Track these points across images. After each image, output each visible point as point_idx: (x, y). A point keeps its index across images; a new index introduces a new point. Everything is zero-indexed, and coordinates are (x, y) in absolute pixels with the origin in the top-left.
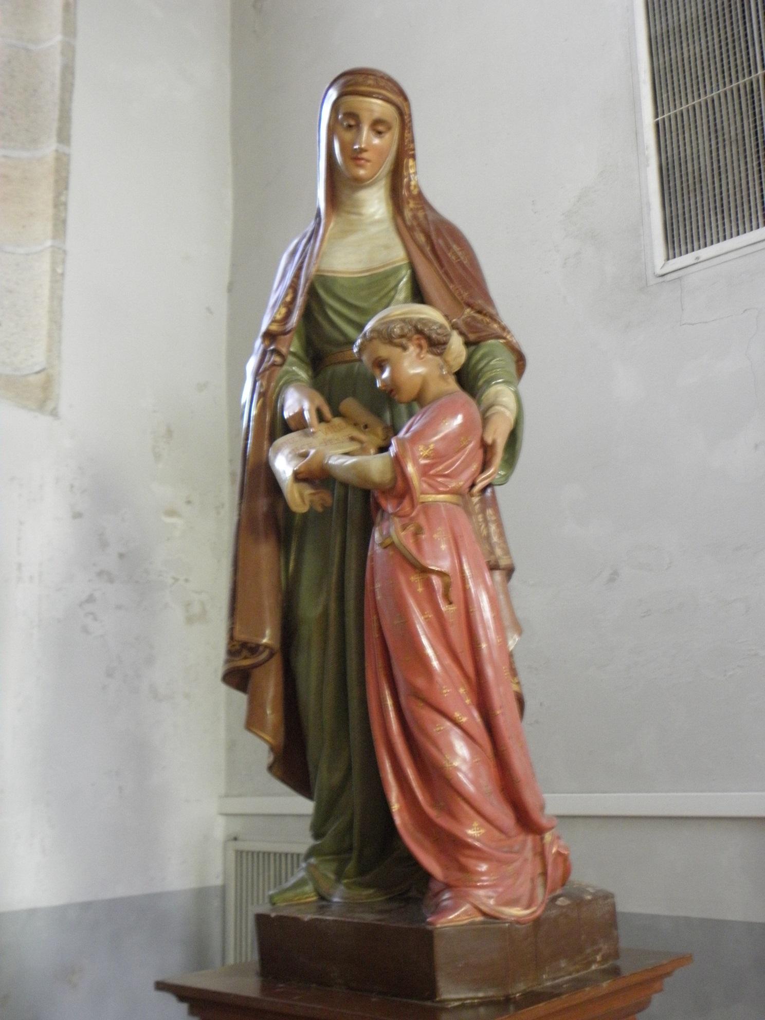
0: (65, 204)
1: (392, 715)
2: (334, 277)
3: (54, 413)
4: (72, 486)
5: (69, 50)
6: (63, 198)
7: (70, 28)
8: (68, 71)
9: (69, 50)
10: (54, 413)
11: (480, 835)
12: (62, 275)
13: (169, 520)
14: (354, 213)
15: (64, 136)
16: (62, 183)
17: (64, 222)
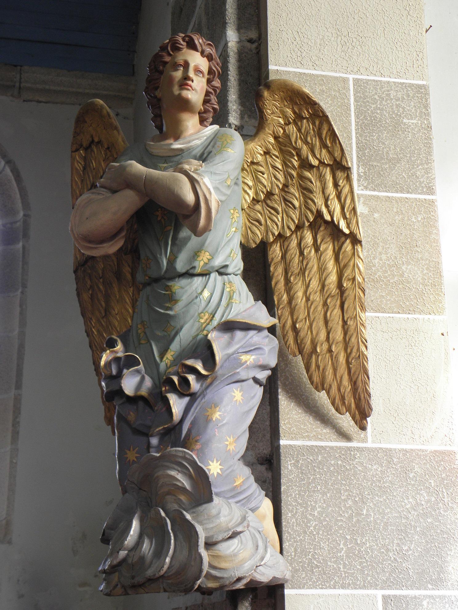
0: (18, 422)
1: (291, 206)
2: (114, 239)
3: (10, 542)
4: (18, 581)
5: (22, 334)
6: (18, 420)
7: (23, 323)
8: (22, 346)
9: (22, 334)
10: (10, 542)
11: (171, 80)
12: (16, 463)
13: (81, 589)
14: (215, 550)
15: (18, 386)
16: (17, 411)
17: (18, 433)
